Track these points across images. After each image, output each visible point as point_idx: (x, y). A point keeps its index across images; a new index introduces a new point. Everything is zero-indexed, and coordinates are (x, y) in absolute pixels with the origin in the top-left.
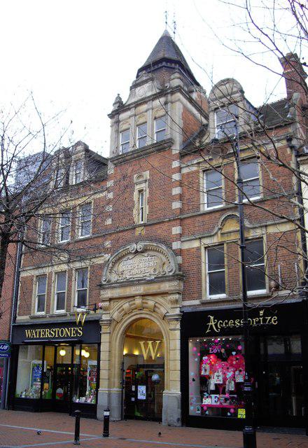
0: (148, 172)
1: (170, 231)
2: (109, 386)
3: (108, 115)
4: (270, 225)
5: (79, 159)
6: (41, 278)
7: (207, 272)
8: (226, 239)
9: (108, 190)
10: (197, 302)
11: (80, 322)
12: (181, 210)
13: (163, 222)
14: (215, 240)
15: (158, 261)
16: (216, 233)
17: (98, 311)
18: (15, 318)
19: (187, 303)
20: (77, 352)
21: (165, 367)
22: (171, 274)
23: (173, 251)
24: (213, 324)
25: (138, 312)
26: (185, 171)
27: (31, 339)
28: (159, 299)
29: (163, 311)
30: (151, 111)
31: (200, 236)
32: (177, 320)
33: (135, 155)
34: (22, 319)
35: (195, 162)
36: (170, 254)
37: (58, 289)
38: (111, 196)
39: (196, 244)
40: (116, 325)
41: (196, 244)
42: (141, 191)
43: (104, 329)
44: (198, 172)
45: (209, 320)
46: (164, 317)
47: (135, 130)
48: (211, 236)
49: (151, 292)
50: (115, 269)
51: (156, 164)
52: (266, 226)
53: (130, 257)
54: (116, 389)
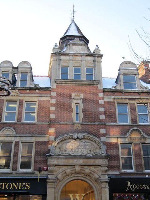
9: (52, 98)
10: (117, 173)
24: (130, 186)
26: (106, 100)
32: (107, 182)
43: (49, 185)
45: (127, 184)
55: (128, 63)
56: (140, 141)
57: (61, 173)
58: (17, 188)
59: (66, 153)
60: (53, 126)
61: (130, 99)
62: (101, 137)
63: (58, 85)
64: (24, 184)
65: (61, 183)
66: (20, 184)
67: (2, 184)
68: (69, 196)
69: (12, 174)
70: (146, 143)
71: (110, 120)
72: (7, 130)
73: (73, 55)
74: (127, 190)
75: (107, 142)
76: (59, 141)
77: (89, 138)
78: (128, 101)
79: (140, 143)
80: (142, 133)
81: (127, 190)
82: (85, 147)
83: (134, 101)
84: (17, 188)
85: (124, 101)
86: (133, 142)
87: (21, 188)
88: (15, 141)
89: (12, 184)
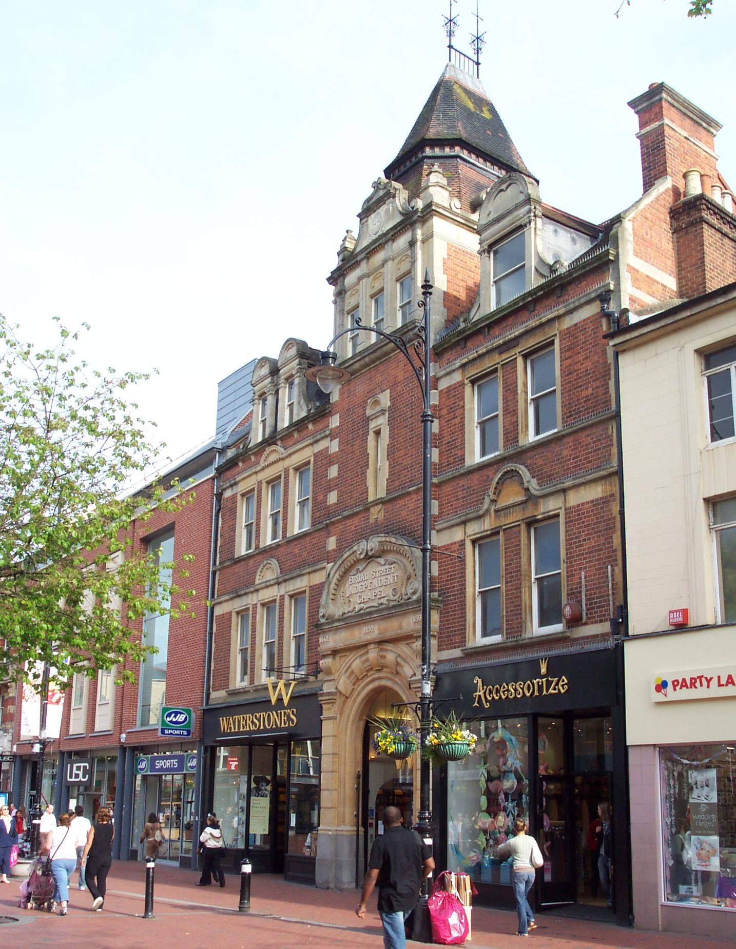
3: (328, 279)
4: (570, 488)
5: (292, 376)
6: (242, 613)
9: (332, 436)
10: (457, 653)
11: (280, 700)
13: (409, 493)
14: (487, 525)
15: (400, 573)
18: (208, 695)
24: (481, 693)
25: (376, 676)
27: (231, 734)
30: (390, 263)
31: (463, 518)
33: (367, 359)
34: (218, 696)
35: (458, 364)
37: (267, 638)
38: (334, 446)
39: (457, 535)
40: (344, 702)
41: (457, 535)
48: (480, 517)
52: (564, 491)
54: (348, 828)
65: (350, 701)
66: (282, 711)
70: (539, 517)
76: (337, 576)
79: (519, 525)
85: (487, 364)
88: (310, 587)
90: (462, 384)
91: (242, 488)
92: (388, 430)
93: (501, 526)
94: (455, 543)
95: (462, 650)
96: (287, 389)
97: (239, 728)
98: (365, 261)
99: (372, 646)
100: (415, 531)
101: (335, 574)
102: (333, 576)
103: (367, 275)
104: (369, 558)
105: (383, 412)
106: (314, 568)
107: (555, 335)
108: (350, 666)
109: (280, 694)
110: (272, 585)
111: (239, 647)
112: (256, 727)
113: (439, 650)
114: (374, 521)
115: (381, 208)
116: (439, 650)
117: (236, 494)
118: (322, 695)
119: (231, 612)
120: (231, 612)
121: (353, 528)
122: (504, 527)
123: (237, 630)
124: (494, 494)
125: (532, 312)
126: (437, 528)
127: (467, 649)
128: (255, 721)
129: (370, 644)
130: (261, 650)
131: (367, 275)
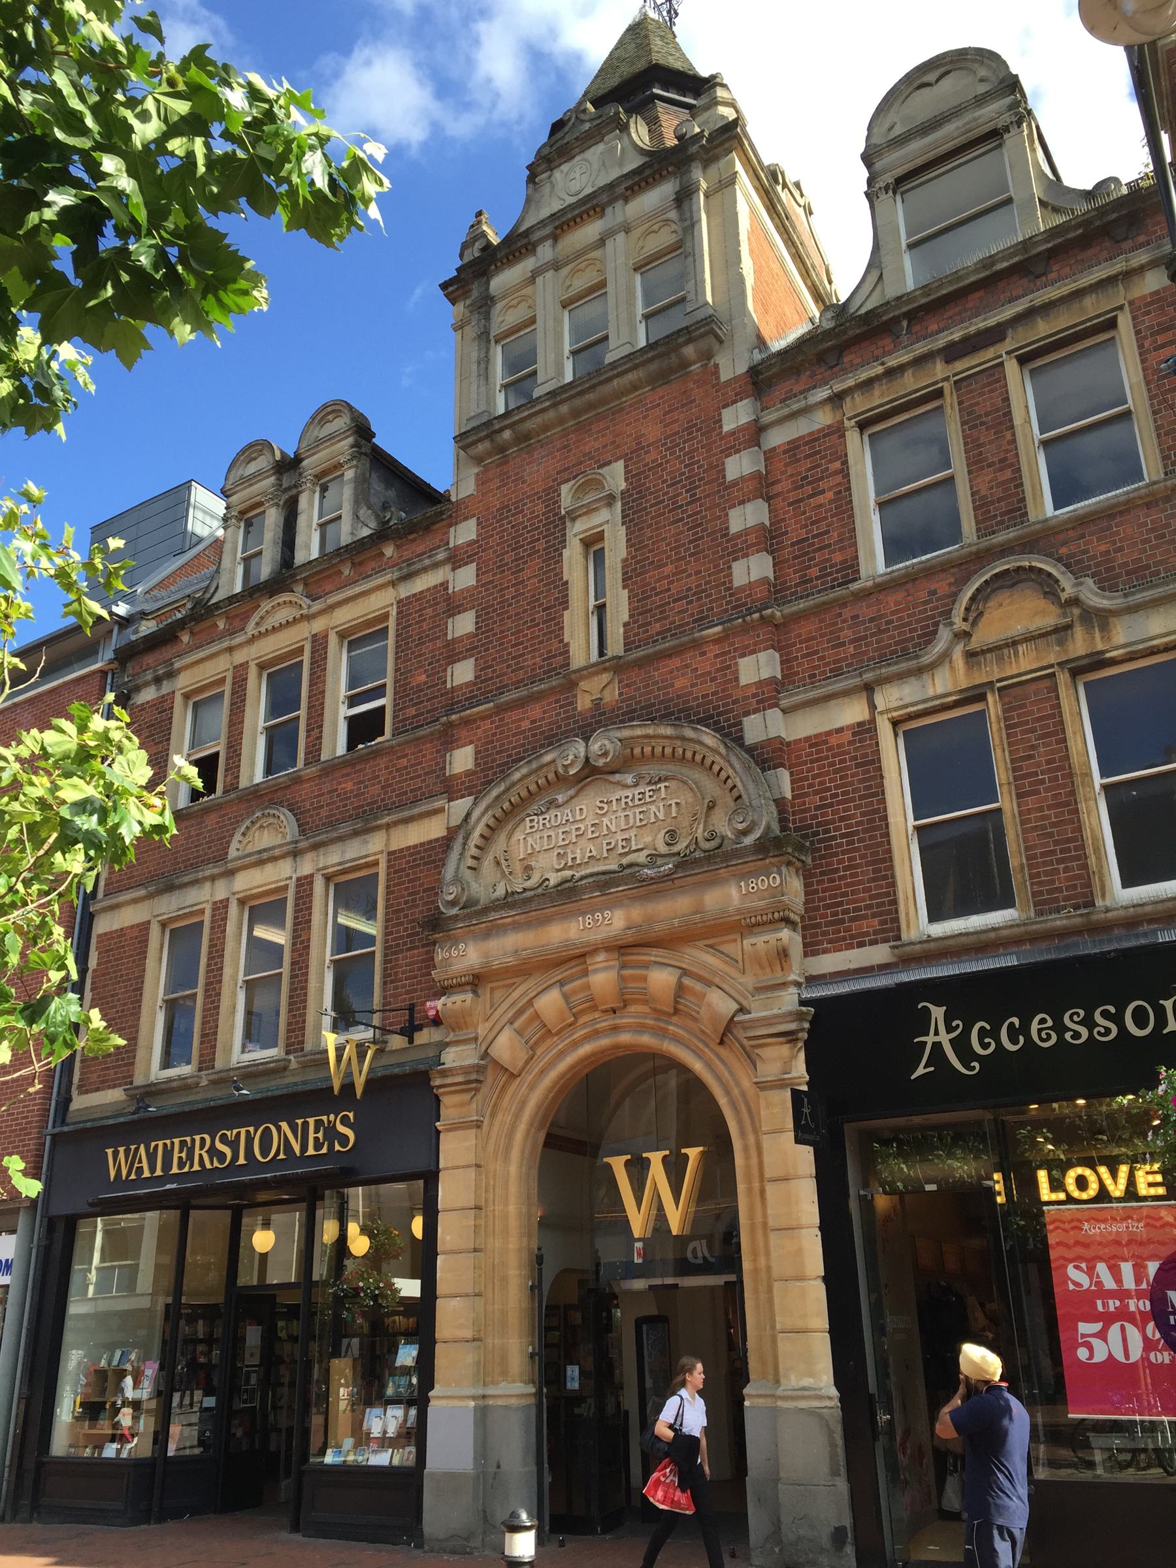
0: (619, 466)
1: (729, 672)
2: (484, 1373)
3: (444, 286)
7: (911, 822)
8: (990, 672)
9: (456, 560)
10: (879, 954)
11: (349, 1087)
12: (777, 590)
16: (946, 656)
17: (422, 1037)
19: (830, 962)
20: (329, 1231)
21: (746, 1265)
22: (748, 841)
23: (750, 750)
24: (944, 1038)
26: (777, 438)
28: (701, 957)
29: (721, 1004)
30: (620, 237)
32: (789, 1037)
35: (822, 394)
36: (736, 768)
38: (465, 578)
39: (852, 712)
41: (852, 712)
42: (593, 544)
43: (451, 1108)
44: (838, 431)
45: (923, 1023)
46: (727, 1032)
47: (558, 322)
49: (659, 928)
50: (500, 844)
51: (652, 431)
53: (561, 798)
55: (931, 77)
56: (1052, 656)
57: (511, 1022)
58: (297, 1148)
59: (528, 884)
60: (464, 733)
61: (952, 353)
62: (747, 714)
63: (486, 469)
64: (329, 1122)
66: (311, 1121)
67: (239, 1134)
68: (609, 1166)
69: (287, 1073)
71: (815, 572)
72: (261, 827)
73: (548, 230)
74: (921, 1071)
75: (797, 741)
76: (487, 819)
77: (533, 788)
78: (939, 370)
79: (1053, 675)
80: (1068, 586)
81: (921, 1071)
82: (635, 815)
83: (990, 353)
84: (297, 1148)
85: (910, 383)
86: (991, 684)
87: (318, 1145)
88: (390, 853)
89: (279, 1129)
90: (838, 431)
91: (184, 681)
92: (622, 531)
93: (991, 683)
94: (839, 730)
95: (892, 947)
96: (317, 495)
97: (167, 1165)
98: (549, 243)
99: (601, 957)
100: (719, 715)
101: (483, 814)
102: (479, 819)
103: (556, 266)
104: (590, 773)
105: (610, 500)
106: (406, 814)
107: (1121, 308)
108: (530, 1003)
109: (349, 1074)
110: (274, 859)
111: (241, 977)
112: (222, 1161)
113: (806, 955)
114: (588, 704)
115: (592, 149)
116: (806, 955)
117: (173, 692)
118: (444, 1073)
119: (149, 922)
120: (149, 922)
121: (526, 725)
122: (998, 685)
123: (160, 959)
124: (965, 620)
125: (1038, 277)
126: (784, 703)
127: (904, 945)
128: (220, 1146)
129: (595, 951)
130: (234, 994)
131: (556, 266)
